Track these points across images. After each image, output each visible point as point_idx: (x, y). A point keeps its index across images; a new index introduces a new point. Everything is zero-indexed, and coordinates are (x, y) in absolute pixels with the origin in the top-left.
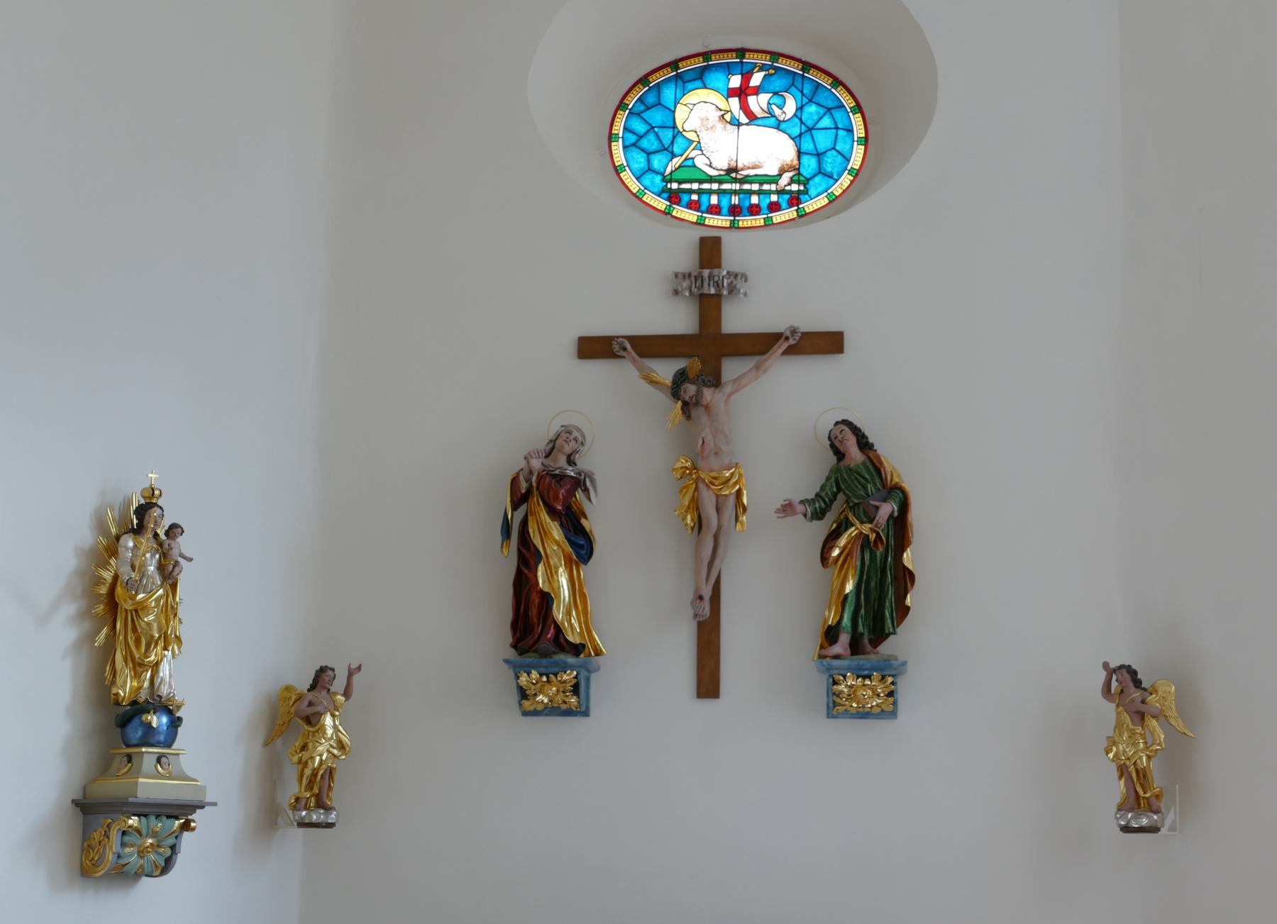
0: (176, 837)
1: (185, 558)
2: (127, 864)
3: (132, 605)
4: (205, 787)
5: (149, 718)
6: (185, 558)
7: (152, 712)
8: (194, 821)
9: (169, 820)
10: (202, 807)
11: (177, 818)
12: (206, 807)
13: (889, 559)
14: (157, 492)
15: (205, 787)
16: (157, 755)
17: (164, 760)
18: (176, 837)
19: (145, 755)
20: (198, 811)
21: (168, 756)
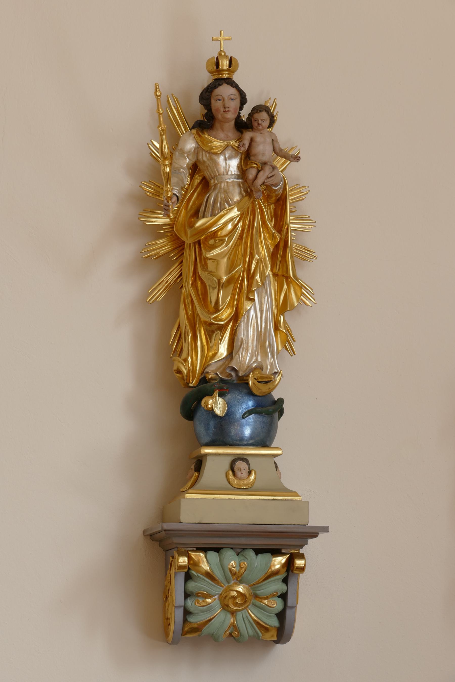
0: (285, 581)
1: (286, 157)
2: (210, 620)
3: (192, 236)
4: (308, 503)
5: (211, 401)
6: (286, 157)
7: (216, 393)
8: (302, 556)
9: (260, 556)
10: (314, 535)
11: (277, 552)
12: (319, 535)
13: (279, 213)
14: (224, 64)
15: (308, 503)
16: (230, 459)
17: (240, 464)
18: (285, 581)
19: (209, 458)
20: (310, 541)
21: (249, 459)
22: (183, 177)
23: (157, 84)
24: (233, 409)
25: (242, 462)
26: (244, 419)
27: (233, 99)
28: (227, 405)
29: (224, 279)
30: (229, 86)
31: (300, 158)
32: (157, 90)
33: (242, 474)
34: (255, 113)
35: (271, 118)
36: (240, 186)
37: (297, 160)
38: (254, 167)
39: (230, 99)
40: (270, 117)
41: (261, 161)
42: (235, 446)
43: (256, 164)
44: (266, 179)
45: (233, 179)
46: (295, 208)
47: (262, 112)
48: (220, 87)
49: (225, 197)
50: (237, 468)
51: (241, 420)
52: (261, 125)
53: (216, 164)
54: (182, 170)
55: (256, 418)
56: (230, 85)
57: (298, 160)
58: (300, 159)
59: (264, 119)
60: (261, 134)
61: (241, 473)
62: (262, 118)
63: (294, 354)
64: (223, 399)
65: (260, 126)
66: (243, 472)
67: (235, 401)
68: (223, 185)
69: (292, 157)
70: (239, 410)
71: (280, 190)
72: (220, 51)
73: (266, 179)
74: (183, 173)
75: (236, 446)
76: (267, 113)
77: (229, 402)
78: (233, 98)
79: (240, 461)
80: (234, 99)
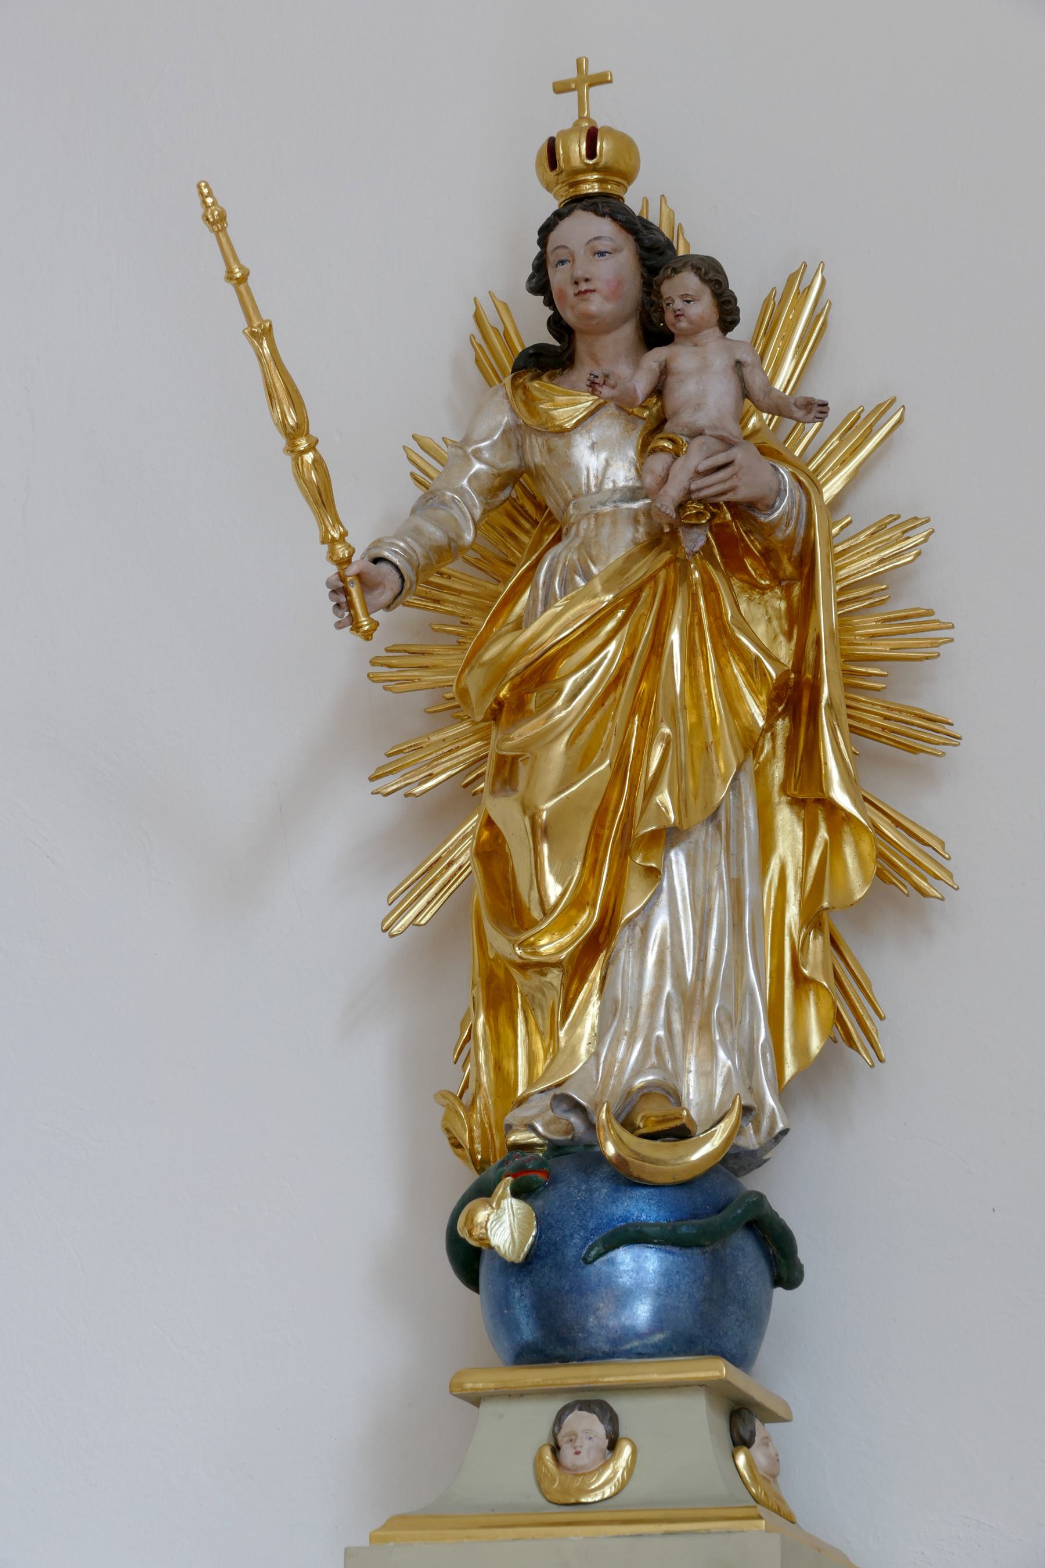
22: (457, 516)
23: (203, 184)
24: (556, 1235)
25: (585, 1413)
26: (589, 1266)
27: (602, 254)
28: (535, 1223)
29: (543, 810)
30: (590, 213)
31: (825, 405)
32: (204, 202)
33: (577, 1453)
34: (663, 281)
35: (713, 288)
36: (636, 521)
37: (820, 415)
38: (663, 449)
39: (595, 254)
40: (710, 288)
41: (687, 427)
42: (575, 1362)
43: (672, 441)
44: (691, 478)
45: (615, 502)
46: (883, 589)
47: (680, 272)
48: (563, 221)
49: (579, 560)
50: (564, 1437)
51: (579, 1270)
52: (683, 315)
53: (569, 465)
54: (449, 493)
55: (636, 1259)
56: (592, 211)
57: (821, 412)
58: (829, 409)
59: (689, 293)
60: (696, 345)
61: (574, 1451)
62: (682, 293)
63: (881, 1060)
64: (530, 1205)
65: (682, 318)
66: (581, 1447)
67: (565, 1209)
68: (585, 527)
69: (795, 404)
70: (576, 1236)
71: (788, 525)
72: (577, 118)
73: (692, 480)
74: (453, 505)
75: (578, 1360)
76: (695, 273)
77: (546, 1212)
78: (602, 249)
79: (579, 1410)
80: (608, 252)
